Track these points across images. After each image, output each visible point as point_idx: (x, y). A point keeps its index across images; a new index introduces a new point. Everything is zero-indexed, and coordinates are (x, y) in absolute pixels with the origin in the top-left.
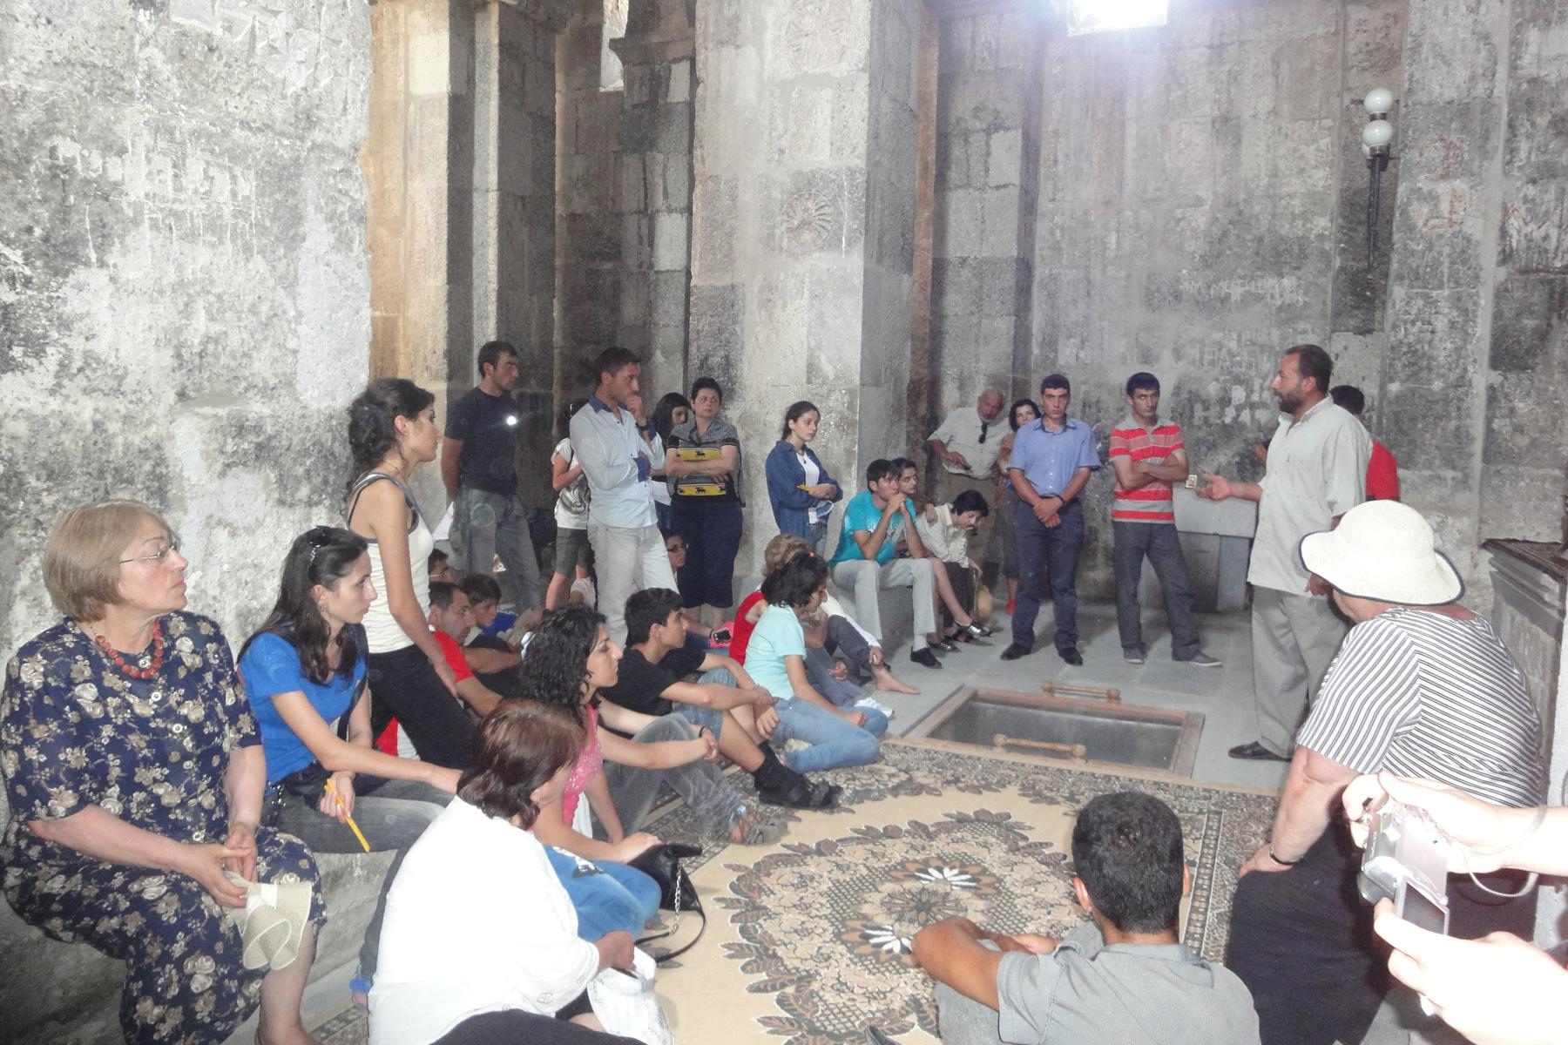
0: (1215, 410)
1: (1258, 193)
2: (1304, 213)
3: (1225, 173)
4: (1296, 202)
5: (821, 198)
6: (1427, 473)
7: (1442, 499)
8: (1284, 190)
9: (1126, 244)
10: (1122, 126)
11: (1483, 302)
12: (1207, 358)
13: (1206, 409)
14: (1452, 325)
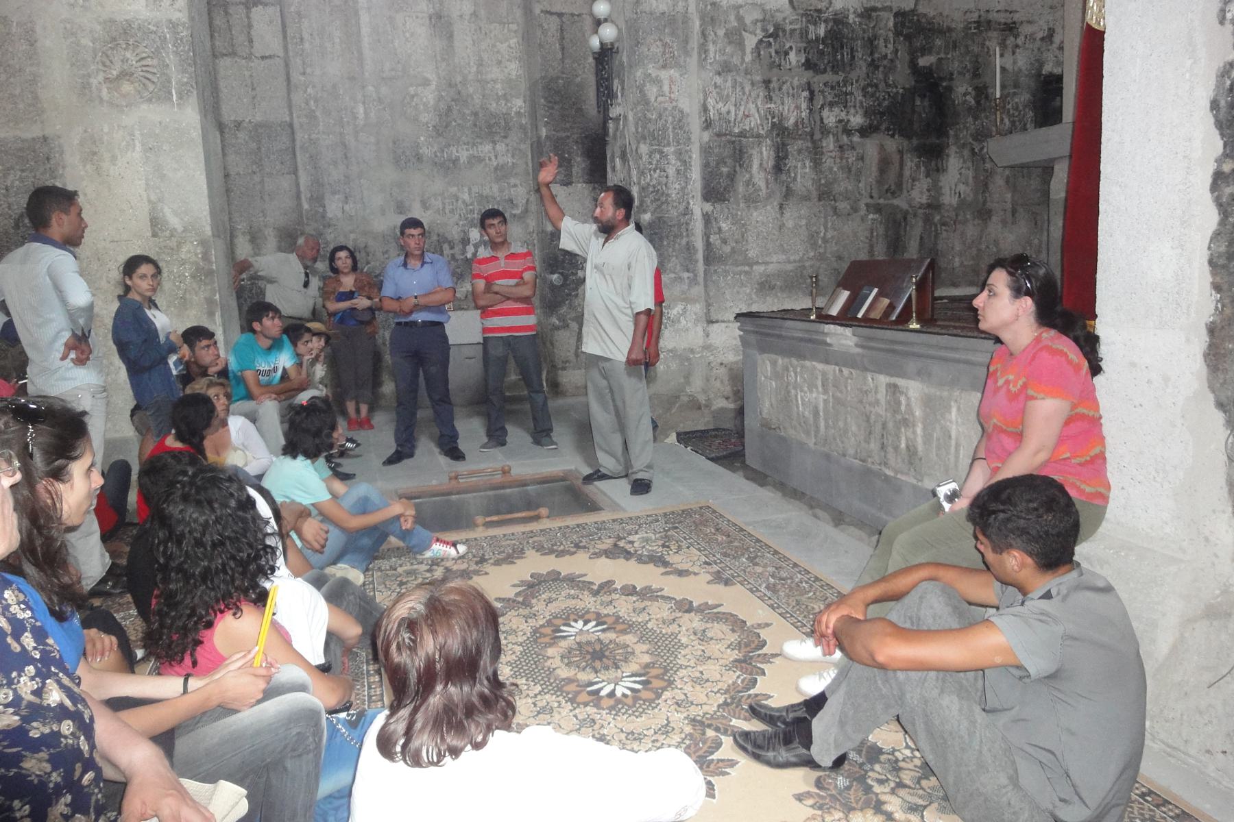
0: (457, 250)
1: (470, 77)
2: (505, 95)
3: (443, 60)
4: (499, 86)
5: (141, 48)
6: (673, 275)
7: (683, 292)
8: (489, 77)
9: (372, 115)
10: (356, 13)
11: (694, 156)
12: (448, 208)
13: (452, 248)
14: (678, 171)
